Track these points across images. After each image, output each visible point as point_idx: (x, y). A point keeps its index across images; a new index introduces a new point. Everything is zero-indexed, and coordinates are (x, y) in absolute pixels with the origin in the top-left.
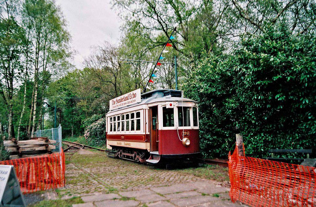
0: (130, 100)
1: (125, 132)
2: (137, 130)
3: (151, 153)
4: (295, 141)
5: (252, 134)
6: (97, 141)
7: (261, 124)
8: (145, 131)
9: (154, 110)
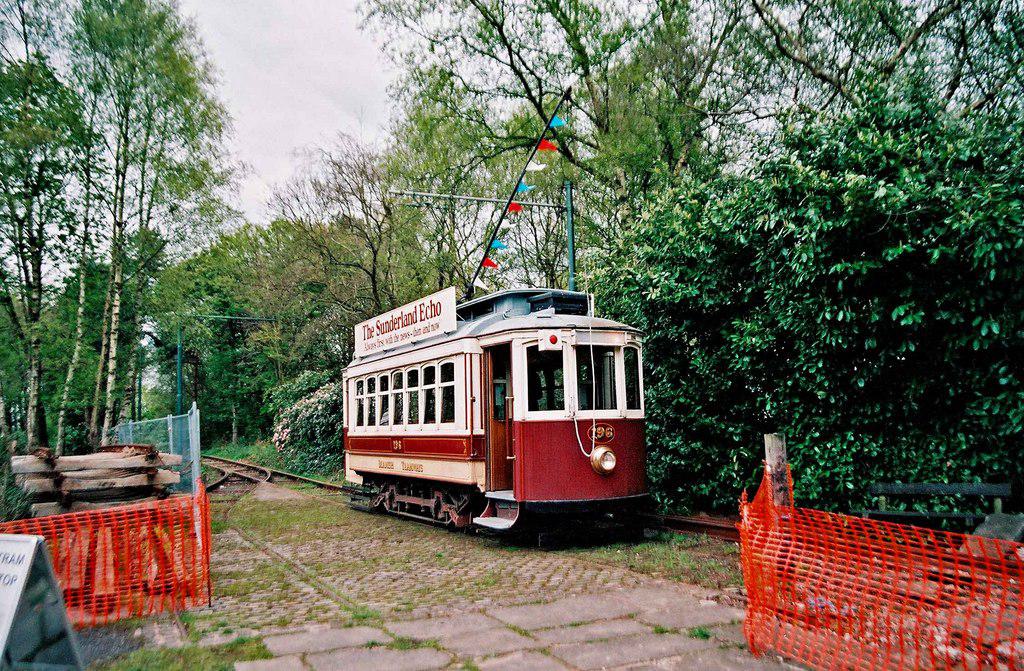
0: (420, 325)
1: (407, 429)
2: (444, 420)
3: (489, 495)
4: (954, 458)
5: (817, 434)
6: (315, 458)
7: (844, 403)
8: (469, 426)
9: (499, 358)
